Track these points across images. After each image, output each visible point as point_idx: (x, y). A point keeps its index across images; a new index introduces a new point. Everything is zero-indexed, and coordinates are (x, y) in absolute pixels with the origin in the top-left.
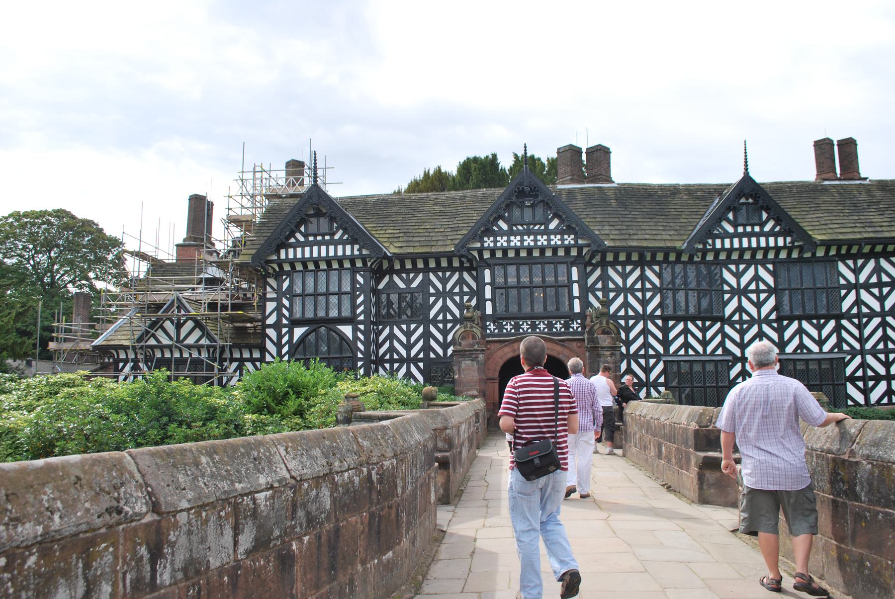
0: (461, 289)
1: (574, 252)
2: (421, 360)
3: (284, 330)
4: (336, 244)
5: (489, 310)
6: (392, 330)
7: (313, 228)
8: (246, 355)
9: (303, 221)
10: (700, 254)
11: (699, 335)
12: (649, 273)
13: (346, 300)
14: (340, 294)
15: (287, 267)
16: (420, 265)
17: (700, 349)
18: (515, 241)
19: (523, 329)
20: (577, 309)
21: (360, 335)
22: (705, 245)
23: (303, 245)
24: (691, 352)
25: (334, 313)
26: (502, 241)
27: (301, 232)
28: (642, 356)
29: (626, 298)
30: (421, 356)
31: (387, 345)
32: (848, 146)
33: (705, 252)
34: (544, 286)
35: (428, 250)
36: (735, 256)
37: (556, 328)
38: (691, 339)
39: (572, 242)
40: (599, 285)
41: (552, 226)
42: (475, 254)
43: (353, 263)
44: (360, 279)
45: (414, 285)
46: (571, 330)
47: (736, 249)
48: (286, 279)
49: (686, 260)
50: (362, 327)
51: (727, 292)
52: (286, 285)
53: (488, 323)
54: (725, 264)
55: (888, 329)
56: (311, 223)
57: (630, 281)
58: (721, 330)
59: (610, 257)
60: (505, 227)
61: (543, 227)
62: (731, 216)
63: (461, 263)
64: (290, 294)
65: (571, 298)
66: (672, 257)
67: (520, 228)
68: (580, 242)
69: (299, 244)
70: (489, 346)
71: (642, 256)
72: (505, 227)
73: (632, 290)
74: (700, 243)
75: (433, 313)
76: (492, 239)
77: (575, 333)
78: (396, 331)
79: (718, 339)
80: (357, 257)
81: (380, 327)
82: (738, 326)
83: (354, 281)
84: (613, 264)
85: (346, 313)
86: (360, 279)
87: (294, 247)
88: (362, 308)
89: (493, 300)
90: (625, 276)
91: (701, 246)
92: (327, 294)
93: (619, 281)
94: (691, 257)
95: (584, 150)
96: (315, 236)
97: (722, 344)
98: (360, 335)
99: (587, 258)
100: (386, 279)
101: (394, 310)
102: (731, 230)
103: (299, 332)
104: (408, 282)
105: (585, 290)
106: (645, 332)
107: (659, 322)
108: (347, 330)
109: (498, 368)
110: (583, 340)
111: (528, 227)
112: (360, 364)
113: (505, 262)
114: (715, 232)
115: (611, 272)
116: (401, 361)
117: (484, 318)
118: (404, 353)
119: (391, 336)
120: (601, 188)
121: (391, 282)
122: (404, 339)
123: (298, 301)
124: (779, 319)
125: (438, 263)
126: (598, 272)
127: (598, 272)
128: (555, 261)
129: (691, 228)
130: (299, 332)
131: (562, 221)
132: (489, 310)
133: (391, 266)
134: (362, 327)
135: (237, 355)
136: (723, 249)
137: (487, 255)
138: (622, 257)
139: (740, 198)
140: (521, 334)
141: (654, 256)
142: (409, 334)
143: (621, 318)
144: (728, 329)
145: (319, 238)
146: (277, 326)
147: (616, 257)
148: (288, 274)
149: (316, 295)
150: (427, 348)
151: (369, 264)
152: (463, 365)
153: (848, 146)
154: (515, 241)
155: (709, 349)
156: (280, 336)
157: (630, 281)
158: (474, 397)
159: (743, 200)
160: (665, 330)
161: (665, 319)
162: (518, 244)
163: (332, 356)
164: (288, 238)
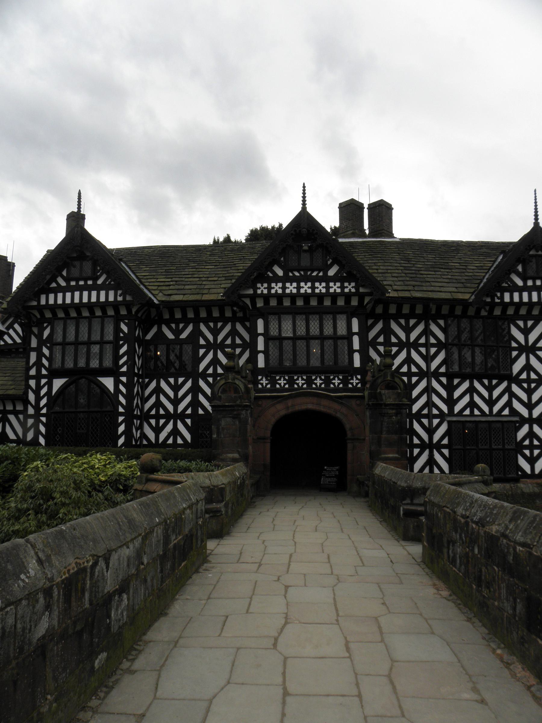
0: (233, 340)
1: (354, 302)
2: (188, 416)
3: (43, 381)
4: (98, 289)
5: (261, 363)
6: (158, 383)
7: (75, 272)
9: (66, 265)
10: (487, 308)
11: (486, 394)
12: (434, 328)
13: (109, 349)
14: (102, 343)
15: (48, 315)
16: (191, 315)
17: (486, 409)
18: (291, 288)
19: (298, 384)
20: (357, 363)
21: (122, 388)
22: (493, 299)
23: (64, 290)
24: (476, 412)
25: (95, 364)
26: (277, 288)
27: (62, 277)
28: (425, 416)
29: (409, 353)
30: (189, 411)
31: (153, 400)
33: (493, 305)
34: (322, 338)
35: (198, 297)
36: (523, 311)
37: (334, 384)
38: (477, 399)
39: (353, 290)
40: (381, 339)
41: (331, 272)
42: (248, 301)
43: (117, 311)
44: (125, 328)
45: (184, 336)
46: (350, 386)
47: (525, 304)
48: (47, 327)
49: (473, 314)
50: (124, 379)
51: (515, 349)
52: (46, 333)
53: (260, 378)
54: (512, 320)
55: (172, 397)
57: (413, 336)
58: (508, 389)
59: (393, 310)
60: (280, 273)
61: (321, 274)
62: (520, 268)
63: (234, 313)
64: (50, 342)
65: (351, 351)
66: (458, 311)
67: (297, 274)
68: (361, 290)
70: (260, 403)
71: (426, 308)
73: (415, 345)
74: (487, 296)
75: (202, 366)
76: (266, 285)
77: (355, 389)
78: (163, 384)
79: (505, 398)
81: (147, 380)
82: (525, 385)
83: (117, 329)
84: (396, 318)
85: (108, 363)
86: (125, 328)
87: (55, 291)
88: (125, 359)
89: (266, 352)
90: (408, 330)
91: (489, 300)
92: (89, 343)
93: (402, 335)
94: (478, 311)
95: (366, 206)
96: (77, 280)
97: (509, 404)
98: (122, 388)
99: (369, 307)
100: (154, 330)
101: (162, 362)
102: (520, 283)
104: (177, 332)
105: (365, 345)
106: (429, 390)
107: (444, 380)
108: (109, 383)
109: (270, 427)
110: (363, 397)
111: (306, 273)
112: (121, 419)
113: (280, 312)
114: (504, 285)
115: (394, 326)
116: (168, 416)
117: (256, 371)
118: (170, 408)
119: (158, 390)
120: (383, 241)
121: (160, 332)
122: (171, 394)
123: (58, 350)
125: (209, 313)
126: (379, 326)
127: (379, 326)
128: (334, 312)
129: (478, 281)
130: (58, 383)
131: (342, 267)
132: (261, 363)
133: (160, 315)
134: (124, 379)
136: (512, 302)
137: (260, 304)
138: (406, 310)
139: (530, 250)
140: (296, 389)
141: (439, 309)
142: (176, 388)
143: (404, 374)
144: (515, 388)
145: (81, 283)
146: (38, 377)
147: (399, 308)
148: (50, 322)
149: (77, 343)
150: (195, 404)
152: (223, 423)
154: (291, 288)
155: (496, 409)
156: (39, 387)
157: (413, 336)
158: (235, 461)
159: (532, 253)
160: (450, 388)
161: (450, 376)
162: (294, 291)
163: (92, 409)
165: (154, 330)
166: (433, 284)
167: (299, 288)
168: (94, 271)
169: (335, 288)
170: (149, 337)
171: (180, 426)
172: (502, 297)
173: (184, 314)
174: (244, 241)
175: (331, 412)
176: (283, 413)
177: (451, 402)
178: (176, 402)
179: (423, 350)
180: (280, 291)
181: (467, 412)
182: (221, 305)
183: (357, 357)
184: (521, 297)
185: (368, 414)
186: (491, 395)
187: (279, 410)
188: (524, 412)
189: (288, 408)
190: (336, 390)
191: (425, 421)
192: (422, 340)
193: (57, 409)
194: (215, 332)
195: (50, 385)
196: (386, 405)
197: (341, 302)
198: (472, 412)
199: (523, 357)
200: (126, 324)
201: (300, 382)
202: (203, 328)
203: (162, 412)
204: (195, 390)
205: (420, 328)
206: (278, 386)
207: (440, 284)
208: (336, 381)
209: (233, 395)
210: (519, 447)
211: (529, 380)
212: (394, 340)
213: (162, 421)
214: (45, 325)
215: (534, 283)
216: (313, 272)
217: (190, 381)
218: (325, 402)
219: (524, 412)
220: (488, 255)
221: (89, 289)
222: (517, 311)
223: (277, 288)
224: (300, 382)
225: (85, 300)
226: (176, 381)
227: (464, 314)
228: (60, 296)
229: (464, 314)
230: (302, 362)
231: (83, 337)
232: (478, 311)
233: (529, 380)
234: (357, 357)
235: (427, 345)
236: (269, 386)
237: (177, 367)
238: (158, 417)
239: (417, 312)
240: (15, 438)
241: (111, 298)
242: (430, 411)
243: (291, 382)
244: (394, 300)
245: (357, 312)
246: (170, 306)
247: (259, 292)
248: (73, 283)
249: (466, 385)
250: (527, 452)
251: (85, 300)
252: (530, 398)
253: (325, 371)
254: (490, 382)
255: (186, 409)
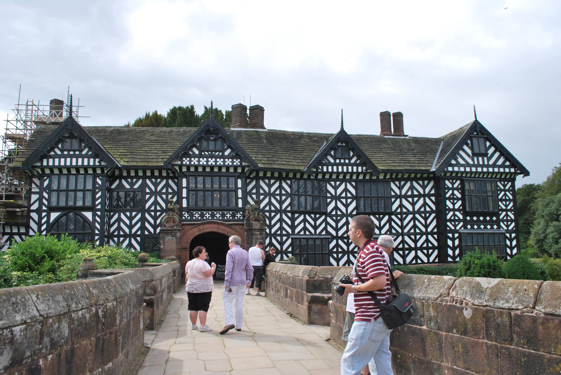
0: (167, 190)
1: (239, 170)
2: (138, 236)
3: (44, 214)
4: (83, 157)
5: (185, 204)
6: (119, 215)
7: (67, 146)
8: (15, 230)
9: (61, 141)
10: (314, 175)
11: (313, 223)
12: (284, 185)
14: (84, 191)
15: (47, 171)
16: (141, 174)
17: (312, 231)
19: (206, 217)
20: (240, 205)
23: (60, 157)
24: (307, 233)
25: (80, 203)
26: (195, 161)
31: (116, 225)
32: (398, 116)
35: (146, 164)
36: (334, 177)
37: (227, 217)
38: (308, 225)
39: (239, 164)
40: (254, 191)
41: (227, 153)
42: (177, 168)
45: (136, 186)
46: (236, 218)
48: (46, 179)
50: (99, 213)
52: (46, 183)
54: (328, 181)
56: (66, 142)
57: (273, 189)
58: (325, 220)
60: (197, 152)
61: (221, 154)
62: (332, 153)
63: (168, 173)
64: (49, 189)
65: (237, 198)
66: (298, 176)
67: (206, 153)
68: (243, 164)
69: (57, 156)
70: (184, 227)
71: (280, 174)
72: (197, 152)
74: (314, 168)
75: (147, 205)
76: (188, 159)
77: (239, 220)
78: (123, 216)
80: (98, 167)
81: (112, 214)
82: (334, 218)
83: (94, 182)
84: (263, 178)
85: (88, 203)
87: (54, 158)
88: (100, 200)
89: (187, 198)
90: (270, 186)
91: (315, 170)
92: (76, 191)
93: (266, 189)
94: (309, 176)
95: (248, 108)
96: (69, 151)
97: (325, 228)
100: (117, 182)
102: (332, 161)
103: (54, 216)
105: (246, 194)
107: (289, 215)
108: (89, 215)
109: (190, 242)
110: (243, 224)
113: (196, 174)
116: (126, 236)
117: (181, 209)
118: (127, 231)
119: (119, 220)
125: (153, 173)
126: (254, 183)
127: (254, 183)
128: (228, 175)
129: (310, 159)
130: (54, 216)
131: (233, 150)
132: (185, 204)
133: (121, 174)
134: (99, 213)
135: (8, 230)
136: (328, 172)
137: (184, 169)
138: (269, 174)
139: (338, 143)
140: (205, 220)
141: (287, 175)
142: (131, 218)
143: (267, 211)
144: (329, 220)
145: (72, 153)
146: (39, 211)
148: (48, 176)
149: (67, 191)
150: (143, 228)
151: (106, 172)
154: (203, 161)
155: (318, 231)
156: (40, 218)
157: (273, 189)
158: (173, 260)
160: (293, 219)
161: (293, 213)
162: (205, 163)
164: (49, 151)
167: (207, 161)
168: (80, 146)
171: (133, 241)
173: (137, 173)
174: (166, 116)
177: (293, 227)
178: (131, 227)
180: (197, 163)
183: (240, 201)
184: (333, 169)
185: (246, 233)
186: (315, 224)
188: (334, 233)
190: (228, 220)
195: (49, 216)
196: (255, 230)
200: (100, 179)
202: (148, 182)
203: (122, 233)
204: (143, 220)
206: (194, 218)
208: (228, 215)
209: (172, 224)
210: (331, 253)
211: (336, 215)
212: (262, 191)
214: (45, 178)
215: (340, 161)
217: (140, 214)
218: (221, 227)
219: (334, 233)
220: (317, 141)
221: (77, 157)
222: (331, 177)
223: (195, 161)
224: (207, 215)
228: (57, 160)
232: (309, 176)
233: (336, 215)
234: (240, 201)
236: (189, 218)
237: (132, 206)
241: (92, 163)
242: (281, 232)
243: (202, 215)
244: (262, 169)
245: (242, 175)
246: (128, 169)
248: (66, 153)
249: (302, 217)
250: (335, 255)
251: (74, 163)
252: (337, 225)
255: (288, 247)
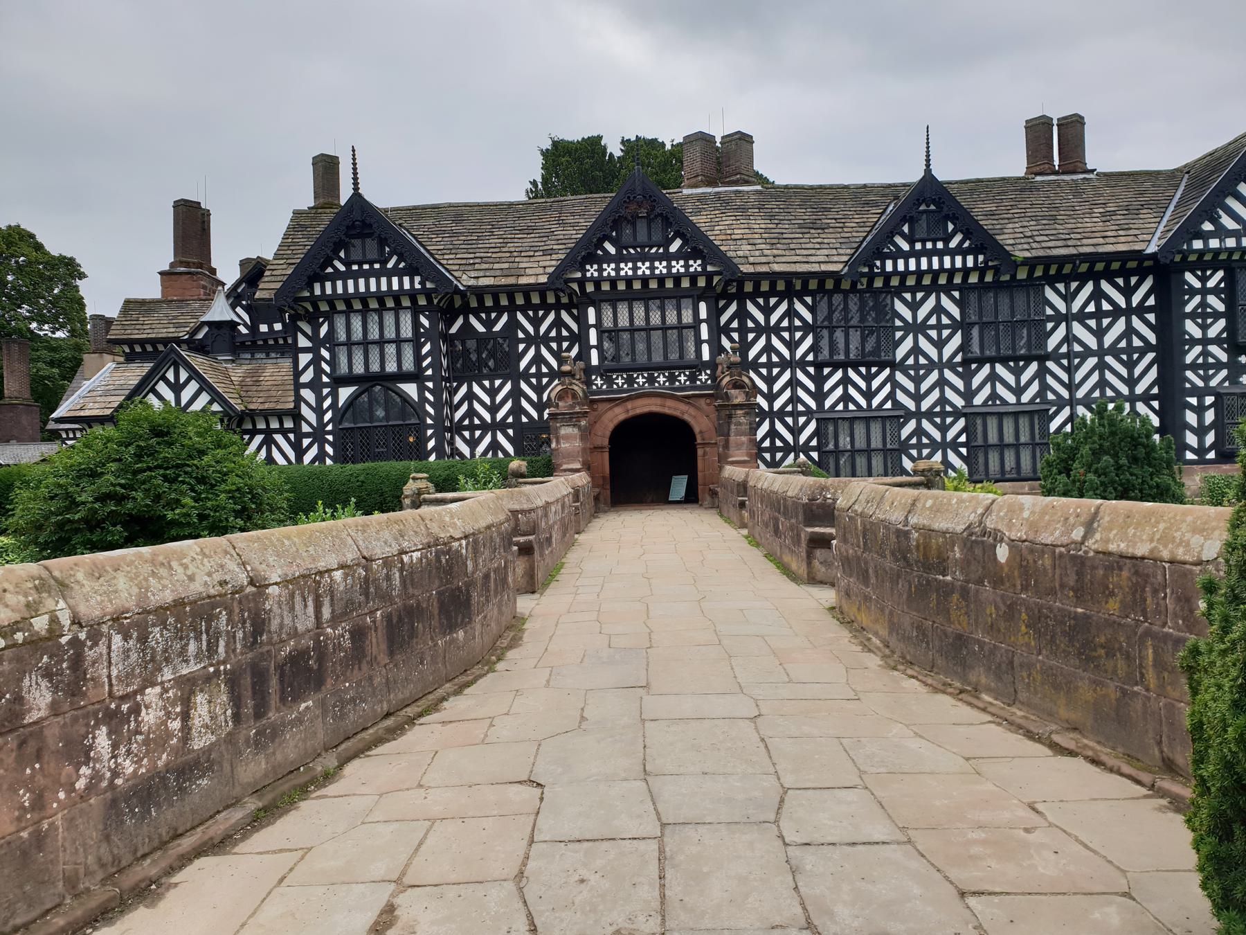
1: (702, 282)
2: (510, 426)
5: (595, 360)
7: (356, 254)
11: (863, 385)
12: (799, 307)
14: (398, 341)
15: (324, 307)
20: (706, 356)
21: (428, 395)
24: (851, 407)
25: (391, 367)
26: (609, 270)
27: (340, 260)
31: (465, 407)
32: (1073, 127)
33: (871, 277)
34: (664, 328)
35: (511, 281)
36: (911, 282)
38: (852, 391)
40: (735, 324)
41: (674, 248)
42: (575, 286)
43: (414, 300)
44: (425, 322)
45: (497, 328)
50: (430, 385)
51: (899, 329)
52: (324, 330)
57: (774, 318)
58: (890, 378)
59: (749, 287)
61: (661, 250)
62: (906, 229)
66: (829, 284)
68: (709, 268)
71: (789, 284)
78: (476, 389)
84: (752, 298)
85: (408, 365)
86: (425, 322)
89: (599, 347)
90: (767, 311)
91: (866, 270)
92: (382, 342)
93: (760, 318)
94: (854, 284)
97: (891, 396)
98: (428, 395)
100: (460, 321)
102: (905, 247)
103: (345, 393)
104: (489, 324)
107: (811, 370)
108: (411, 389)
109: (608, 434)
112: (430, 432)
113: (614, 298)
115: (751, 307)
116: (485, 427)
117: (589, 370)
119: (471, 396)
124: (966, 363)
125: (527, 298)
126: (733, 308)
127: (733, 308)
130: (345, 393)
131: (686, 242)
132: (595, 360)
134: (430, 385)
136: (895, 271)
137: (590, 288)
138: (765, 287)
141: (805, 284)
142: (492, 393)
144: (899, 377)
145: (366, 267)
146: (315, 385)
147: (757, 286)
148: (329, 317)
150: (517, 410)
153: (1073, 127)
155: (876, 402)
159: (923, 207)
160: (819, 380)
161: (819, 366)
165: (460, 321)
166: (798, 252)
169: (678, 267)
170: (453, 330)
172: (883, 265)
175: (677, 413)
176: (622, 417)
177: (819, 396)
178: (493, 409)
179: (786, 335)
180: (613, 274)
181: (840, 407)
182: (542, 289)
183: (705, 349)
187: (619, 414)
188: (911, 405)
189: (628, 411)
191: (789, 420)
192: (785, 323)
193: (346, 425)
194: (536, 323)
197: (685, 283)
198: (846, 406)
199: (910, 338)
201: (641, 380)
205: (784, 307)
207: (805, 252)
212: (750, 324)
213: (478, 433)
216: (651, 248)
218: (669, 403)
219: (911, 405)
222: (903, 281)
224: (641, 380)
225: (373, 288)
226: (492, 384)
227: (837, 288)
229: (837, 288)
230: (642, 359)
231: (374, 334)
234: (705, 349)
235: (792, 329)
238: (472, 428)
239: (779, 288)
240: (1097, 372)
243: (630, 381)
246: (479, 292)
247: (588, 275)
249: (839, 375)
253: (670, 368)
254: (868, 371)
